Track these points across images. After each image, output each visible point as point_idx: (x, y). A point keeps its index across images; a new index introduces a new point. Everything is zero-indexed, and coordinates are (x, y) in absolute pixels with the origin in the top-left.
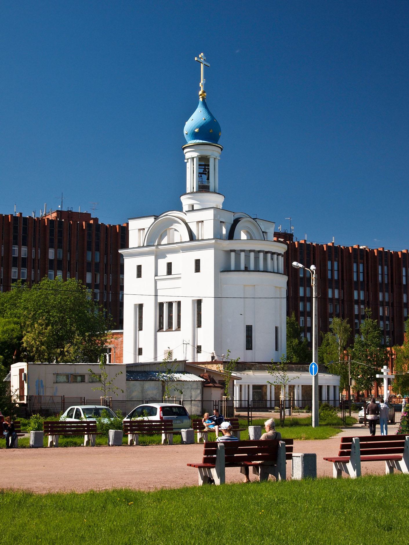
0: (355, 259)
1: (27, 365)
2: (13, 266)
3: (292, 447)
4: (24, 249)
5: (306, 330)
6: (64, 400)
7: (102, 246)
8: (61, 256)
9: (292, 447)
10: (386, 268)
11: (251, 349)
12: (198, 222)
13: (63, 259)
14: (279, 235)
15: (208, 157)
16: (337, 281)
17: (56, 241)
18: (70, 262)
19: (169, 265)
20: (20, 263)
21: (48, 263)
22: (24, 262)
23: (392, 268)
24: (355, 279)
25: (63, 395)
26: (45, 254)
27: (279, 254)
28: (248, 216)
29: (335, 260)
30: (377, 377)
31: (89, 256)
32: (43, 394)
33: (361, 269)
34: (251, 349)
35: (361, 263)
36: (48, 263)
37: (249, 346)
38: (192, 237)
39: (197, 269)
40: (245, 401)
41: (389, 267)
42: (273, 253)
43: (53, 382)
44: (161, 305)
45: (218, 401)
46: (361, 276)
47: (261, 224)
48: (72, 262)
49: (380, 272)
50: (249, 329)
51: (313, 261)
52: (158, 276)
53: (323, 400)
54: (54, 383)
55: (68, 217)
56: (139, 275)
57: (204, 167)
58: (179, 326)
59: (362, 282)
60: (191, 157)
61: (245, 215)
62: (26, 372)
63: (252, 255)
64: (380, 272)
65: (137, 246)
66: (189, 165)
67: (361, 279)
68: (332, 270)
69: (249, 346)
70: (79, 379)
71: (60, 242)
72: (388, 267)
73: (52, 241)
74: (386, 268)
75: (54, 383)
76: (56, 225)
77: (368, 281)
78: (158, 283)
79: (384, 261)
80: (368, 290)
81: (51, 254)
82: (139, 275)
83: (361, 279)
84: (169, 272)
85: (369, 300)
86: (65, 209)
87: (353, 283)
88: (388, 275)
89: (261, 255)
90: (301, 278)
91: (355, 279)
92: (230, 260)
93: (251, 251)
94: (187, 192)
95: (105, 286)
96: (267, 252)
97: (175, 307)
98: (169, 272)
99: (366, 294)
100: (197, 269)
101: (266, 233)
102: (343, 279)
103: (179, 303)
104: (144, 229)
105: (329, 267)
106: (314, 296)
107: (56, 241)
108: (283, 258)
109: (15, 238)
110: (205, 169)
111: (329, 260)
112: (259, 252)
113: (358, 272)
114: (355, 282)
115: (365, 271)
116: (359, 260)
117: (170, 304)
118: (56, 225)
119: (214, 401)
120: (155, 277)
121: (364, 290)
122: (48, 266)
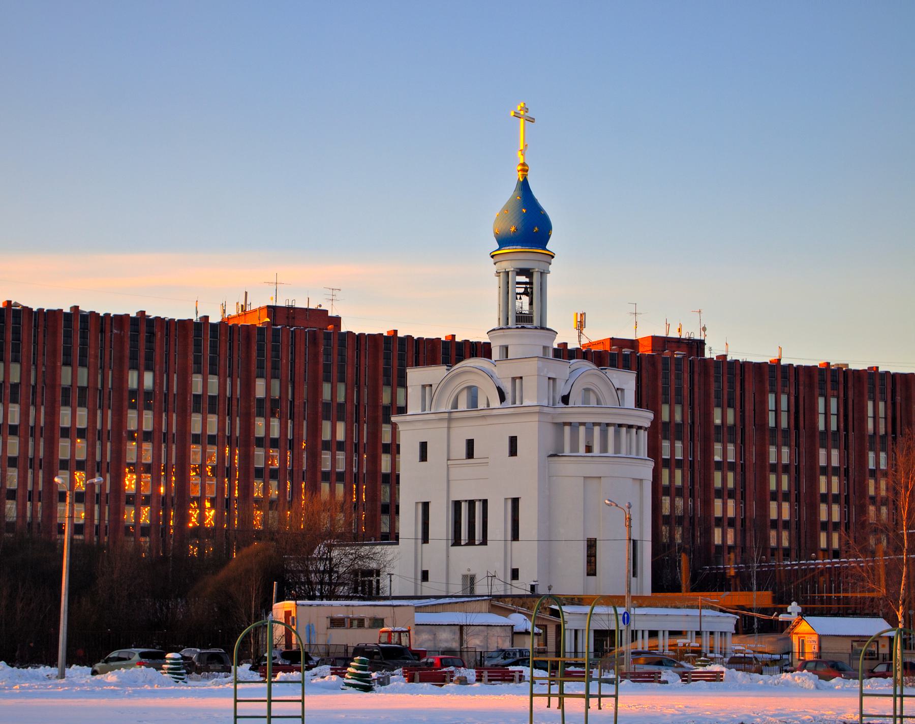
0: (821, 388)
1: (296, 607)
2: (194, 412)
4: (213, 380)
5: (726, 524)
6: (347, 650)
7: (350, 372)
8: (276, 393)
10: (881, 405)
11: (595, 574)
12: (514, 379)
13: (280, 397)
14: (678, 342)
15: (531, 271)
16: (786, 432)
17: (268, 365)
18: (292, 402)
20: (206, 405)
21: (254, 404)
22: (213, 405)
23: (894, 404)
24: (821, 427)
25: (346, 644)
26: (249, 388)
27: (639, 428)
29: (783, 392)
31: (326, 391)
32: (315, 641)
33: (833, 409)
34: (595, 574)
35: (834, 396)
36: (254, 404)
37: (592, 571)
39: (513, 452)
40: (571, 652)
41: (889, 402)
42: (630, 427)
43: (326, 627)
44: (457, 504)
45: (484, 652)
46: (834, 420)
47: (615, 376)
48: (296, 403)
49: (870, 413)
50: (592, 545)
51: (741, 394)
53: (578, 651)
54: (327, 628)
55: (287, 317)
56: (423, 457)
57: (524, 286)
59: (834, 433)
62: (293, 614)
63: (597, 430)
64: (870, 413)
67: (834, 427)
68: (777, 411)
69: (592, 571)
70: (355, 623)
71: (275, 367)
72: (886, 403)
73: (261, 366)
74: (881, 405)
75: (327, 628)
76: (268, 336)
77: (846, 429)
78: (452, 470)
79: (878, 391)
80: (847, 447)
81: (260, 389)
82: (423, 457)
83: (834, 427)
84: (470, 454)
85: (848, 467)
86: (281, 303)
87: (817, 434)
88: (886, 418)
89: (611, 430)
90: (717, 427)
91: (821, 427)
92: (564, 439)
93: (595, 424)
95: (356, 444)
96: (620, 426)
97: (478, 507)
98: (470, 454)
99: (842, 455)
100: (513, 452)
101: (622, 390)
102: (797, 427)
103: (485, 502)
104: (431, 385)
105: (771, 405)
107: (268, 365)
108: (646, 433)
109: (197, 361)
110: (526, 288)
111: (772, 391)
112: (608, 425)
113: (827, 414)
114: (821, 433)
115: (842, 411)
116: (829, 390)
117: (472, 503)
118: (268, 336)
119: (438, 651)
120: (449, 461)
121: (839, 448)
122: (254, 410)
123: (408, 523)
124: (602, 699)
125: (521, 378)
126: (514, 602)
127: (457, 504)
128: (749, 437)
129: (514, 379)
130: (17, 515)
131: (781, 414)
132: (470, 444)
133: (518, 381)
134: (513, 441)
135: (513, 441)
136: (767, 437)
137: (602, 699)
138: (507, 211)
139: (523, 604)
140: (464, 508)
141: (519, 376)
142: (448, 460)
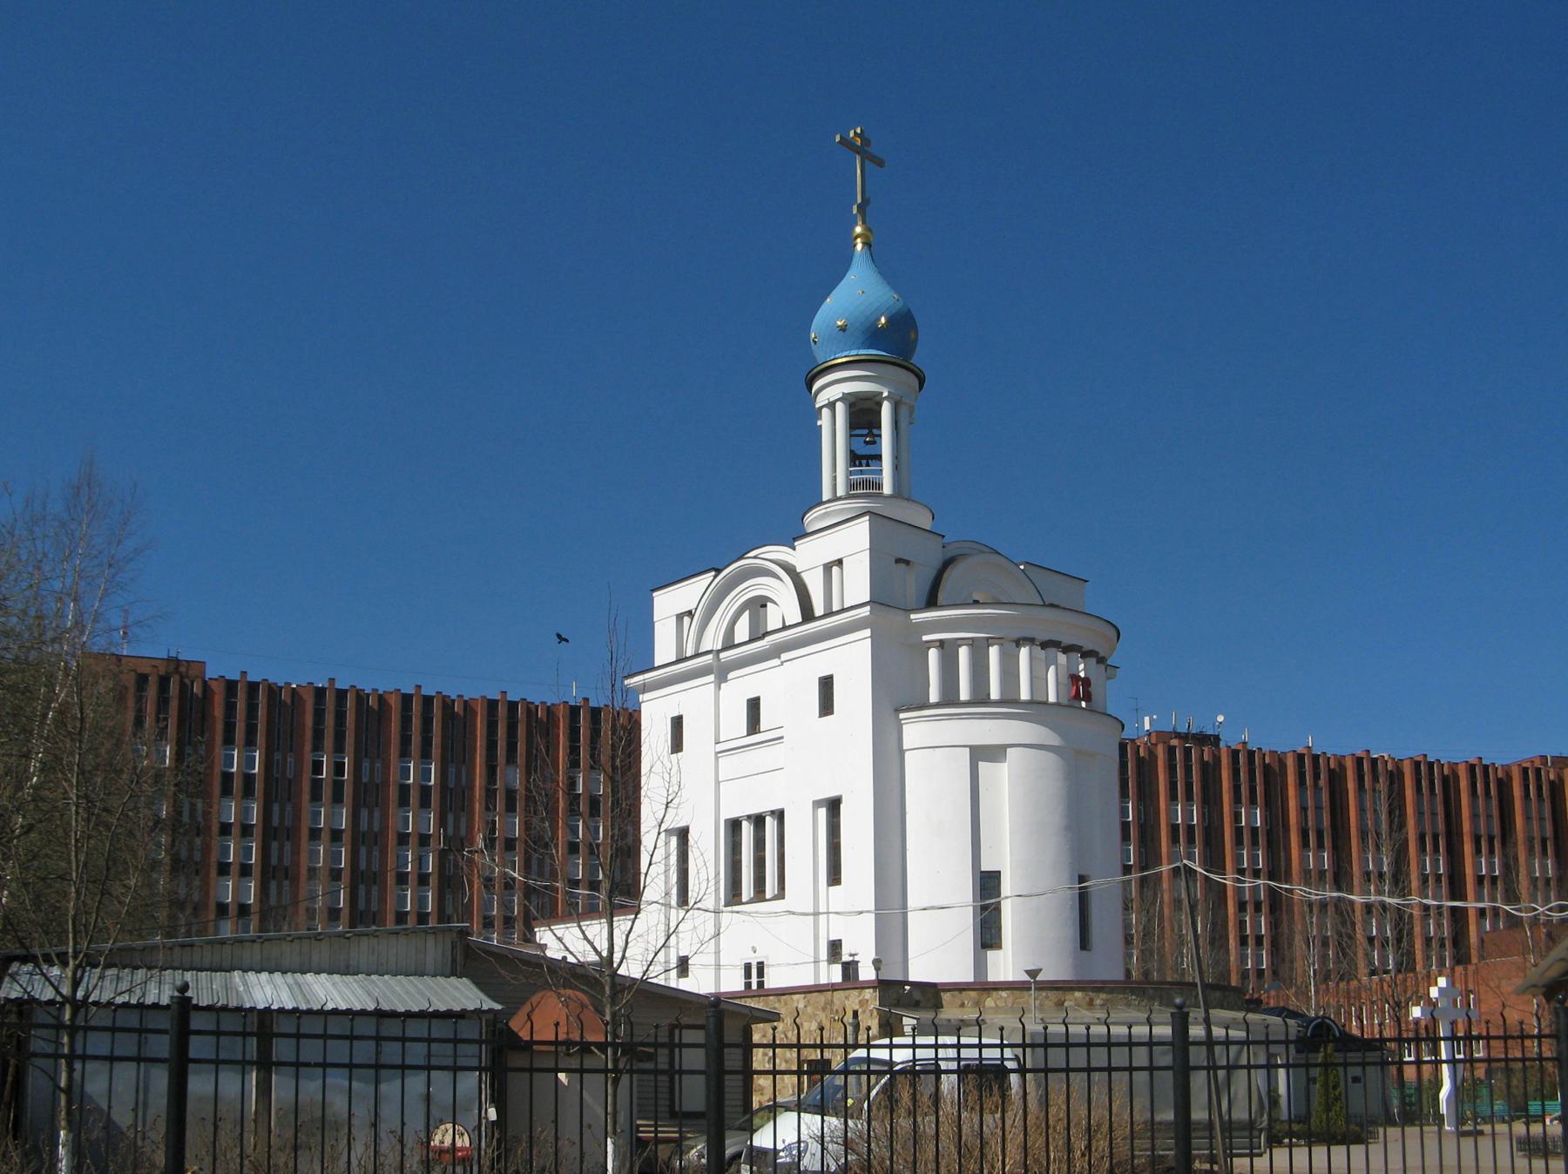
3: (1552, 757)
9: (1552, 757)
19: (754, 706)
28: (986, 550)
30: (1445, 985)
38: (808, 615)
39: (826, 707)
52: (760, 732)
58: (835, 875)
60: (827, 402)
61: (977, 546)
65: (674, 659)
66: (824, 421)
84: (754, 724)
94: (824, 499)
97: (770, 825)
98: (754, 724)
100: (826, 707)
103: (780, 815)
106: (410, 860)
117: (758, 821)
123: (656, 879)
124: (983, 1050)
125: (840, 562)
126: (808, 1001)
127: (734, 826)
128: (944, 944)
129: (828, 568)
130: (260, 909)
131: (708, 1065)
132: (754, 706)
133: (835, 569)
134: (826, 684)
135: (826, 684)
136: (1552, 894)
137: (983, 1050)
138: (863, 292)
139: (826, 1004)
140: (747, 830)
141: (836, 558)
142: (717, 743)
